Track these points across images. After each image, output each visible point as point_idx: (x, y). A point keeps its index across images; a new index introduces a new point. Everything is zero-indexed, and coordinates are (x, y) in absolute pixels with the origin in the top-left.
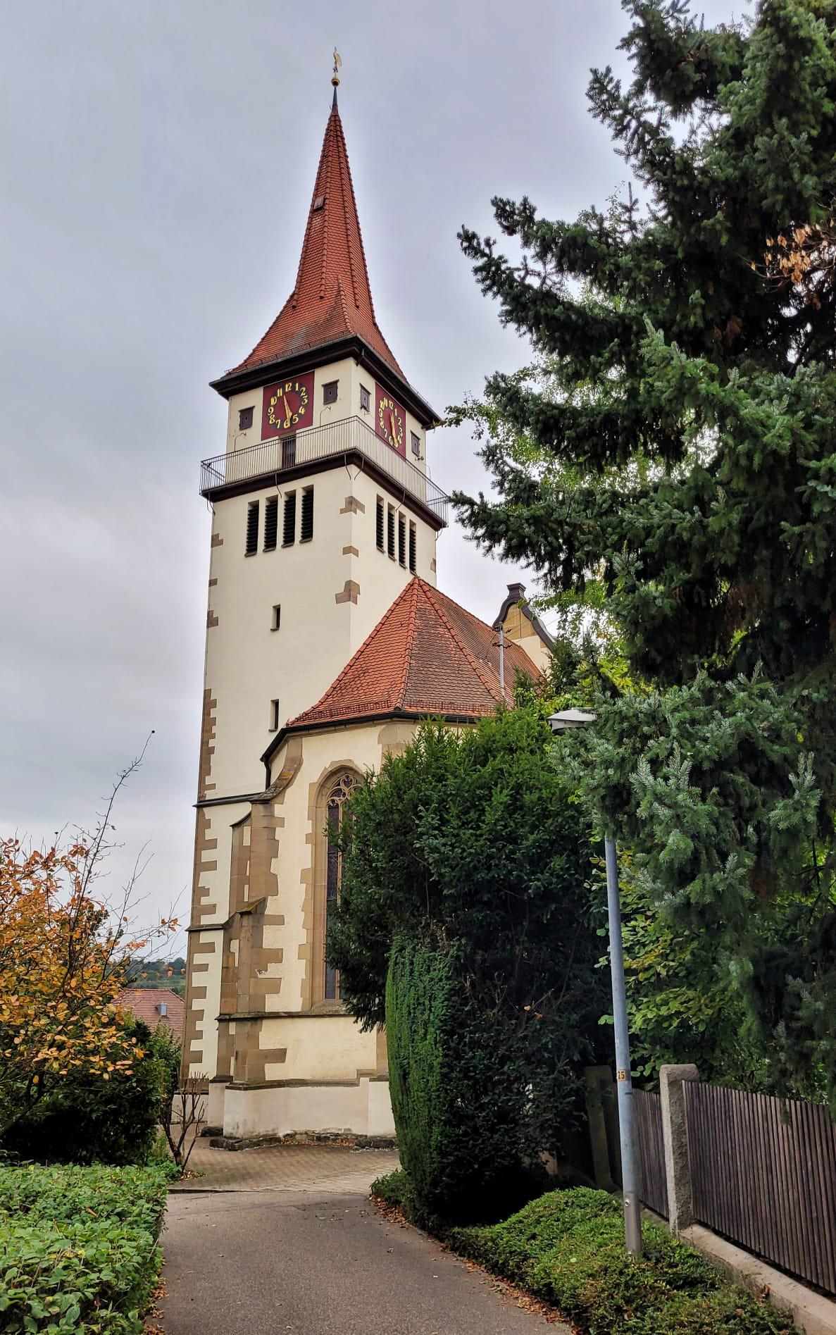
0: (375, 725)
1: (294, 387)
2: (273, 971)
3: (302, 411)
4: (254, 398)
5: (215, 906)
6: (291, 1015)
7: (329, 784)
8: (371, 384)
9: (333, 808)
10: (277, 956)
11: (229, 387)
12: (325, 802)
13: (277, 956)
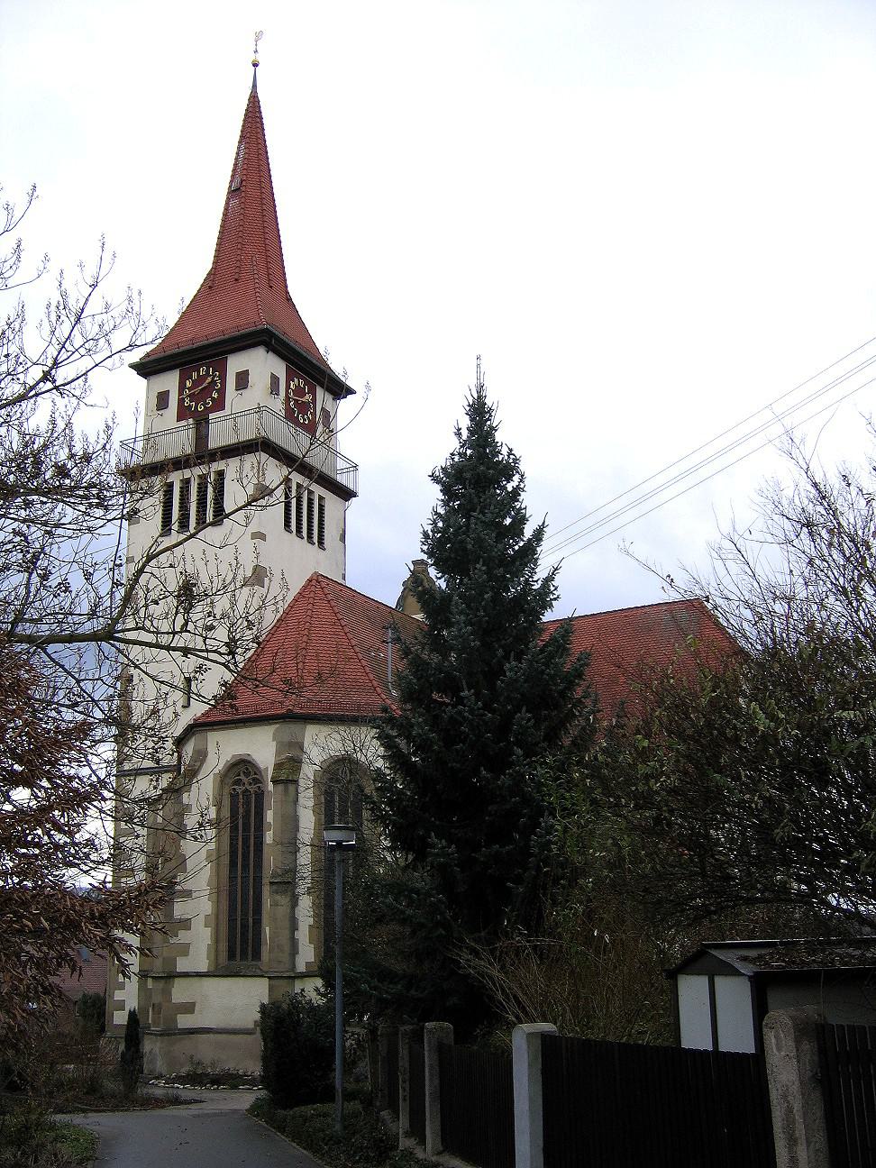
0: (271, 724)
1: (208, 371)
2: (183, 937)
3: (215, 395)
4: (170, 382)
5: (193, 1004)
6: (199, 975)
7: (231, 775)
8: (280, 368)
9: (234, 797)
10: (185, 924)
11: (146, 368)
12: (226, 791)
13: (185, 924)
